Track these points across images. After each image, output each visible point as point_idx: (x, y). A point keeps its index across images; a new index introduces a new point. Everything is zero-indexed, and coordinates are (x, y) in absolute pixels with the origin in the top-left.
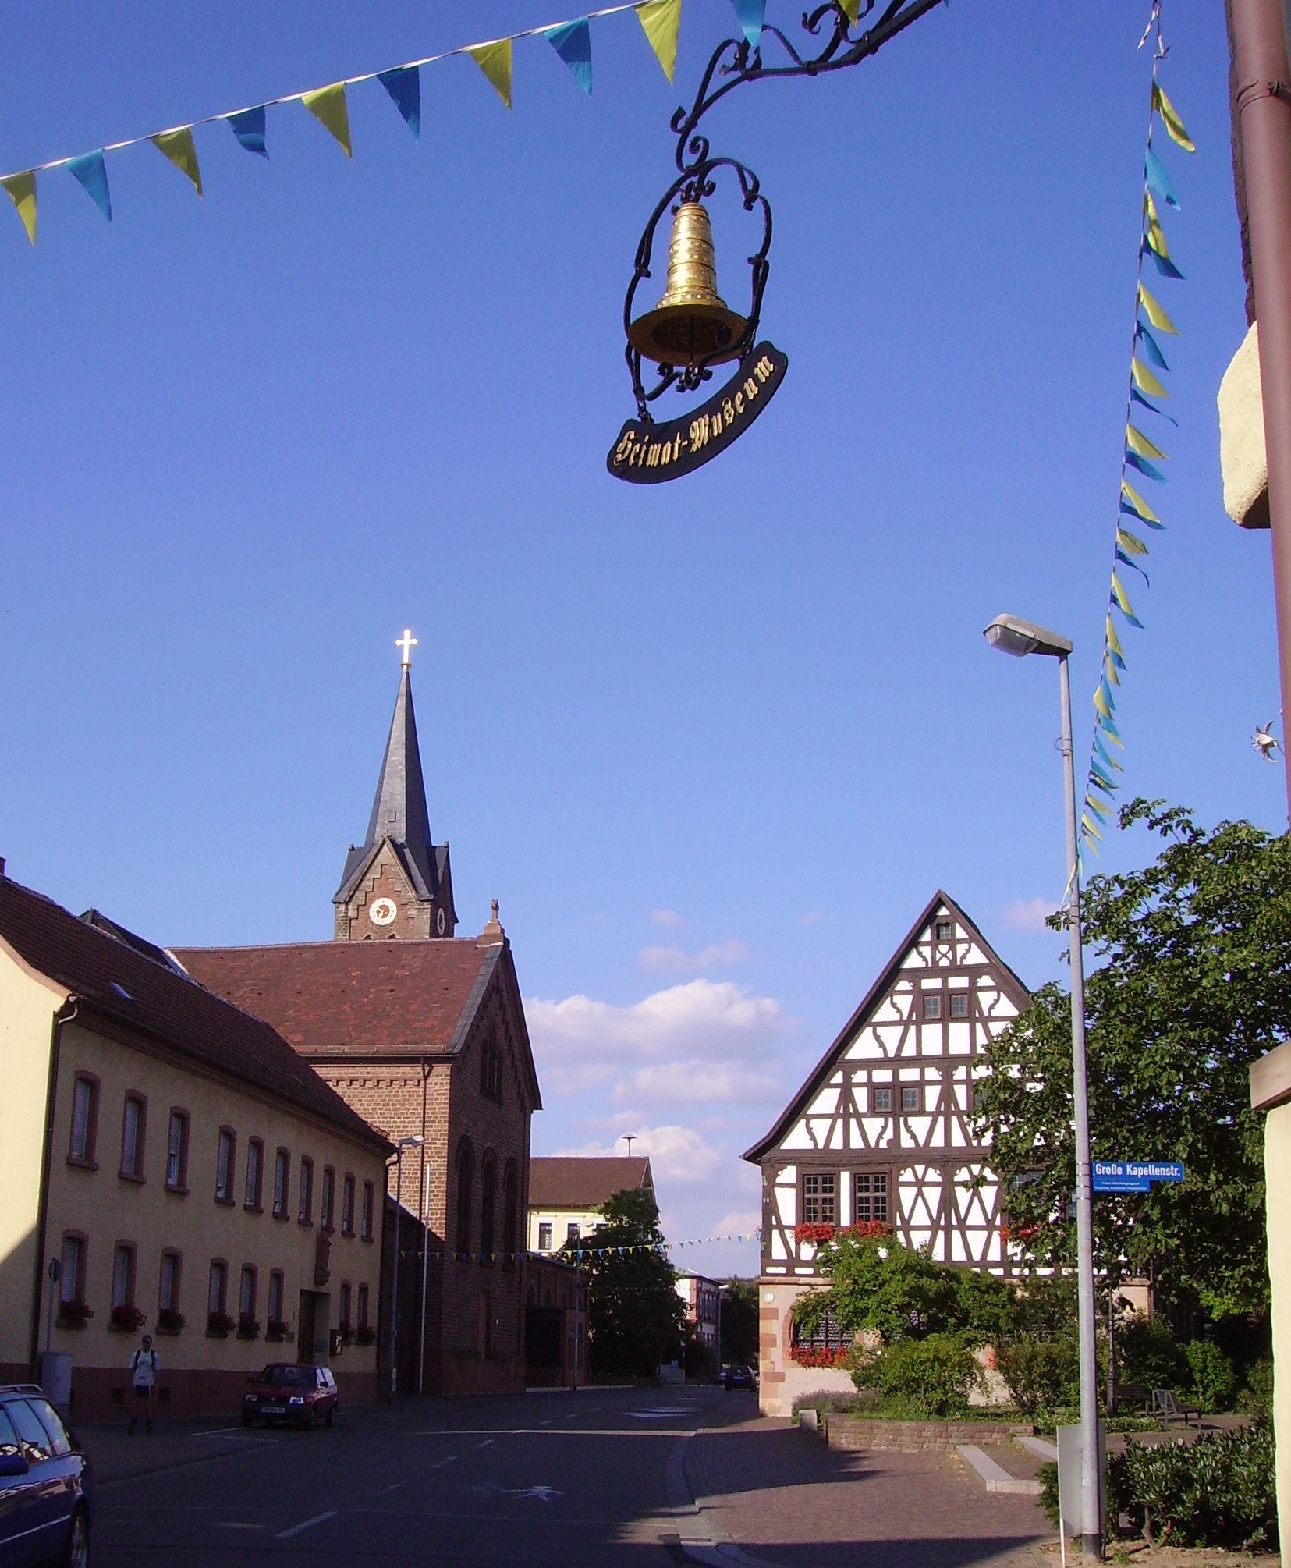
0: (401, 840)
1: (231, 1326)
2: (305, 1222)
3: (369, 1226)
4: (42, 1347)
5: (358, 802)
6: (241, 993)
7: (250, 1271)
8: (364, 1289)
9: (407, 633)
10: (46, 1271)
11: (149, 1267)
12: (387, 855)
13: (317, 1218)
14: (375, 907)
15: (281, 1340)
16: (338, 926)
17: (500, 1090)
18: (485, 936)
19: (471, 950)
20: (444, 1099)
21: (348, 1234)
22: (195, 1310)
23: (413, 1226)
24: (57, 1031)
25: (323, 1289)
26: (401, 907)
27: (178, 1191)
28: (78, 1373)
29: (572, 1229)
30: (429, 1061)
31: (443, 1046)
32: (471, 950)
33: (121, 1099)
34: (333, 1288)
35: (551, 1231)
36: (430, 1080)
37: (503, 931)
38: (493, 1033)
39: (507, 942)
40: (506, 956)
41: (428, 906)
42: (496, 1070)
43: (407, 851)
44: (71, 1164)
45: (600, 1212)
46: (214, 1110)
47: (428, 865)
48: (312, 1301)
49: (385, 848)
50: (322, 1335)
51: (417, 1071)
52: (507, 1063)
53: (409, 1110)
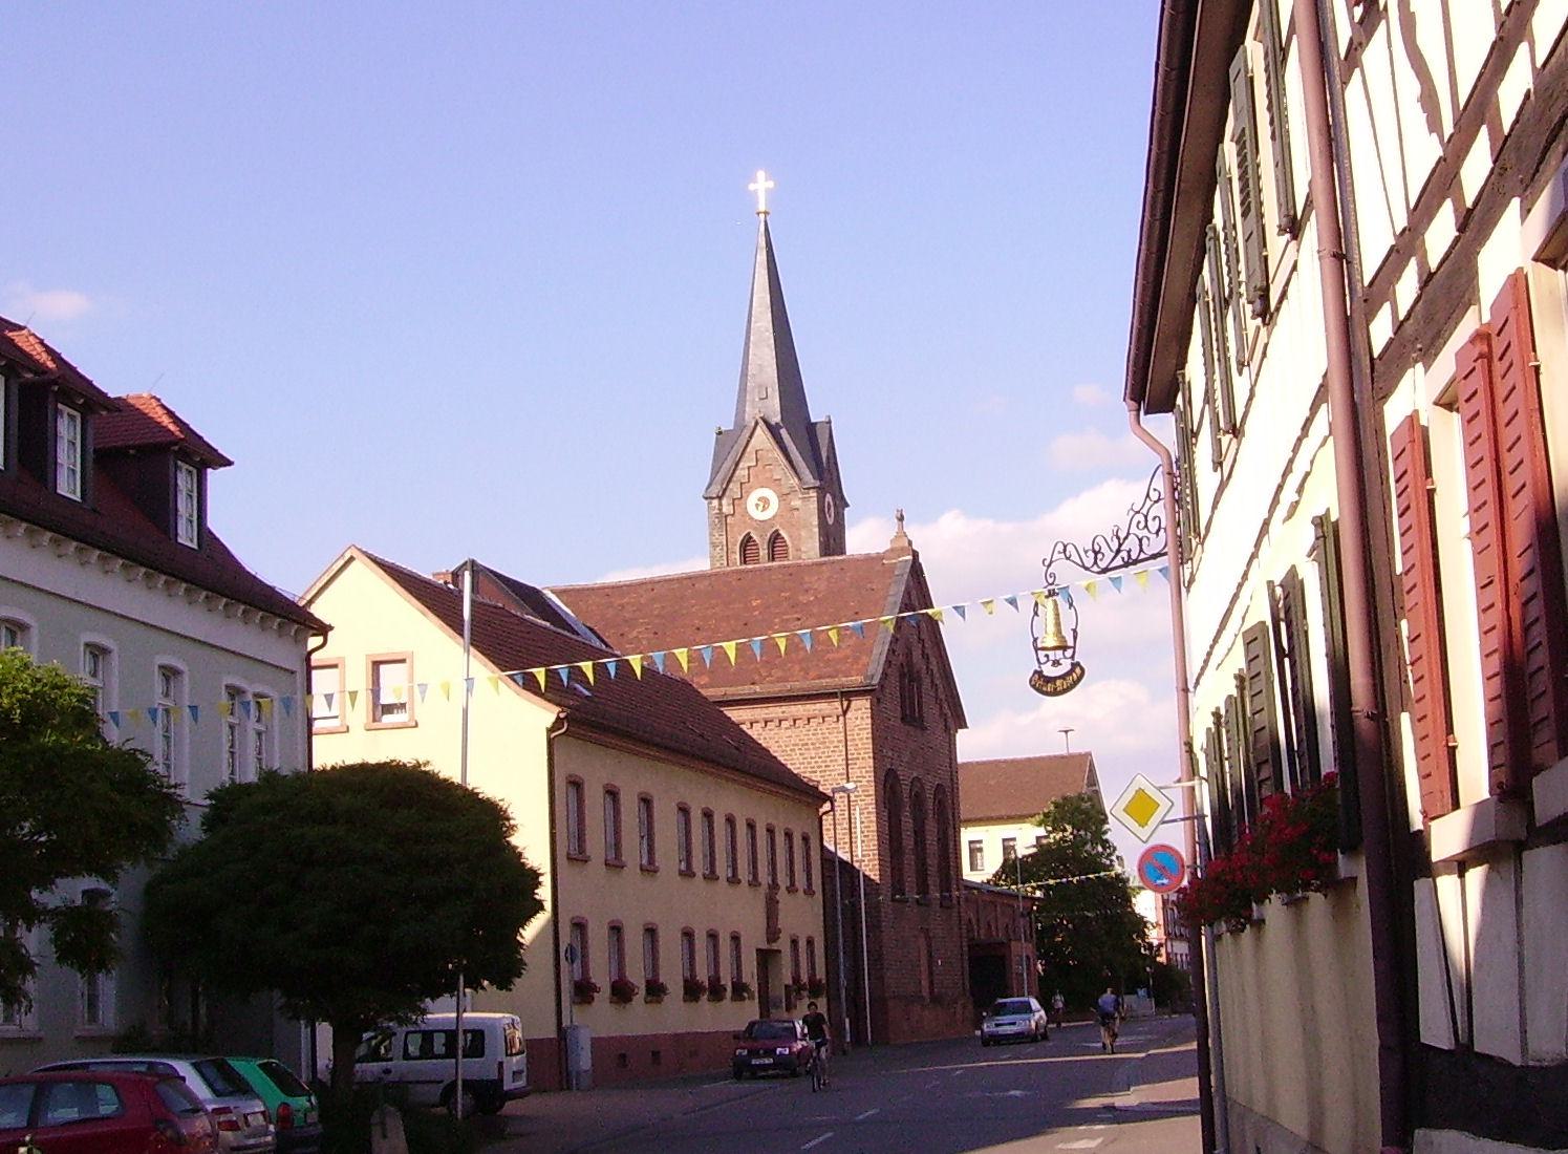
0: (776, 419)
1: (704, 989)
2: (754, 883)
3: (809, 879)
4: (566, 1022)
5: (723, 382)
6: (635, 633)
7: (713, 936)
8: (810, 942)
9: (761, 175)
10: (562, 954)
11: (598, 937)
12: (762, 438)
13: (764, 877)
14: (752, 500)
15: (743, 999)
16: (712, 526)
17: (921, 716)
18: (892, 550)
19: (879, 567)
20: (867, 734)
21: (792, 889)
22: (672, 977)
23: (848, 869)
24: (550, 743)
25: (775, 946)
26: (783, 497)
27: (650, 869)
28: (596, 1042)
29: (1008, 846)
30: (848, 695)
31: (860, 678)
32: (878, 567)
33: (601, 791)
34: (783, 944)
35: (988, 849)
36: (849, 715)
37: (910, 543)
38: (909, 655)
39: (915, 555)
40: (916, 570)
41: (813, 494)
42: (915, 690)
43: (783, 432)
44: (570, 858)
45: (1039, 825)
46: (674, 788)
47: (809, 446)
48: (766, 958)
49: (759, 431)
50: (778, 990)
51: (836, 706)
52: (926, 681)
53: (829, 749)
